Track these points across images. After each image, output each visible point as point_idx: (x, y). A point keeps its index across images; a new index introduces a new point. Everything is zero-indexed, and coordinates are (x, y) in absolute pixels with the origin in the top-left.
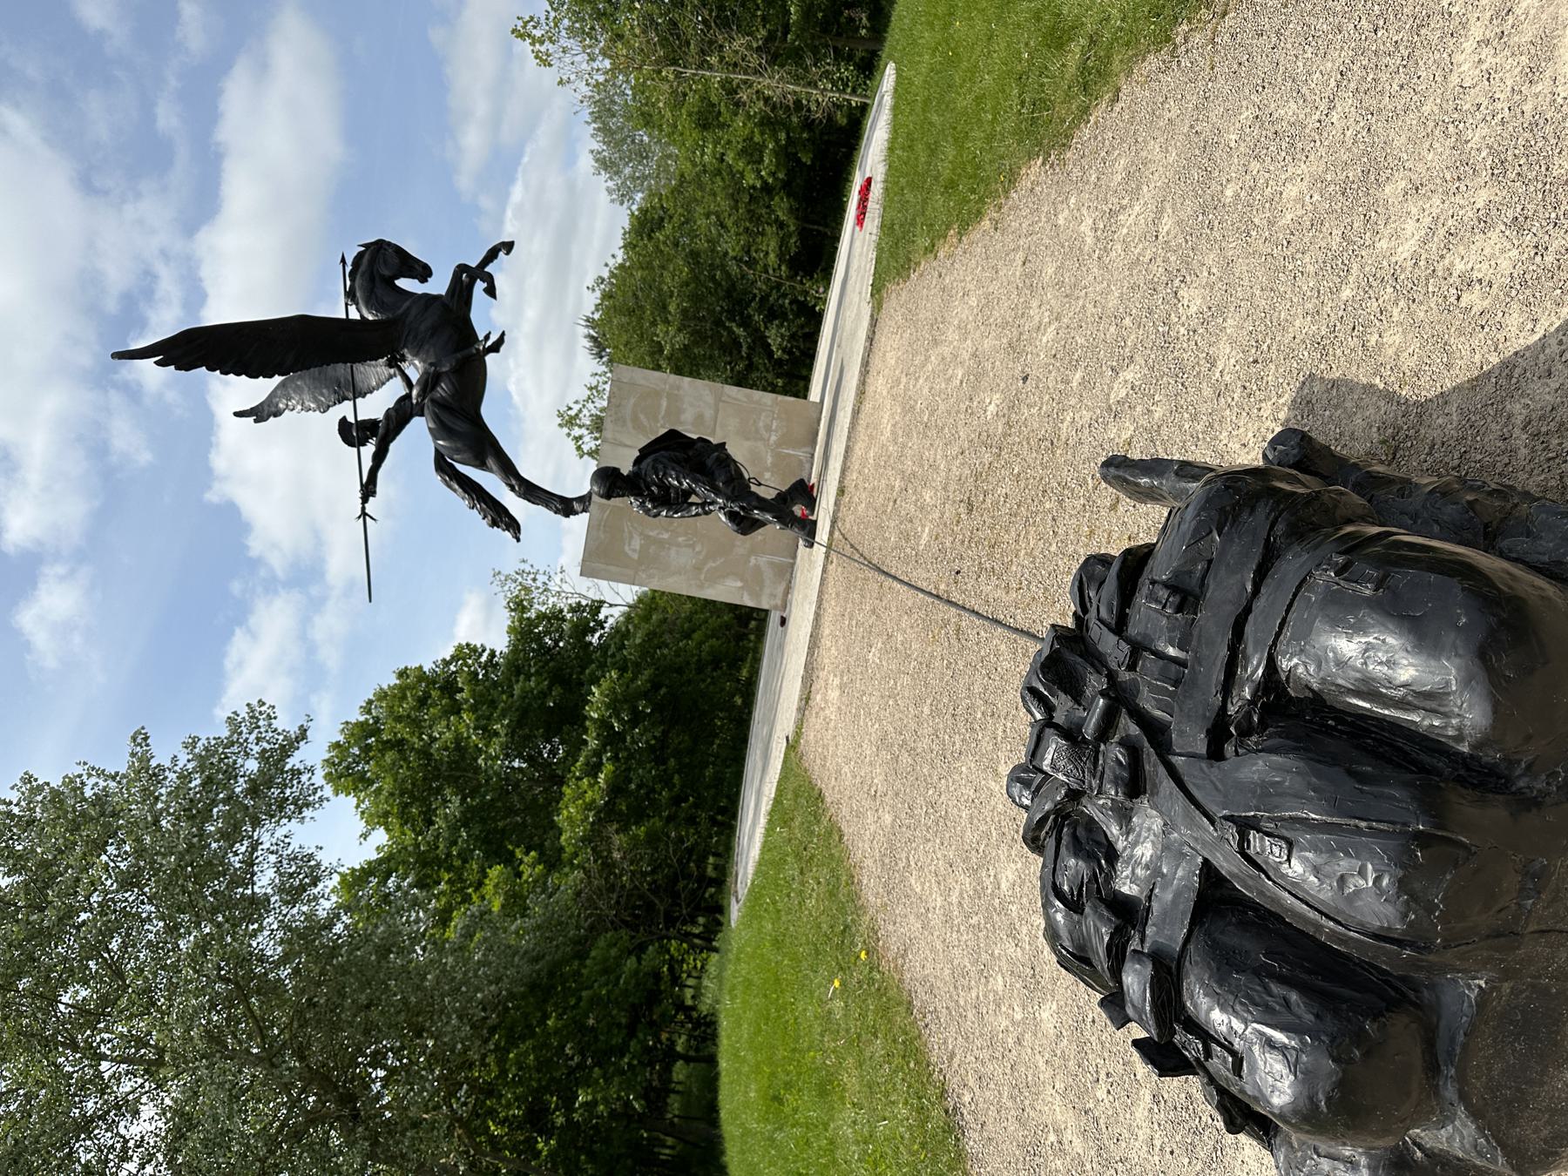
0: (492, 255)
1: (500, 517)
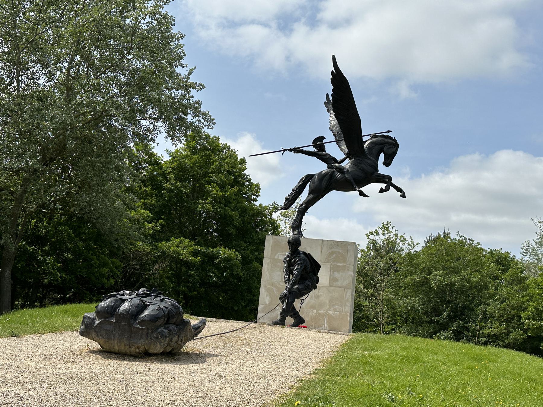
0: (399, 189)
1: (290, 201)
